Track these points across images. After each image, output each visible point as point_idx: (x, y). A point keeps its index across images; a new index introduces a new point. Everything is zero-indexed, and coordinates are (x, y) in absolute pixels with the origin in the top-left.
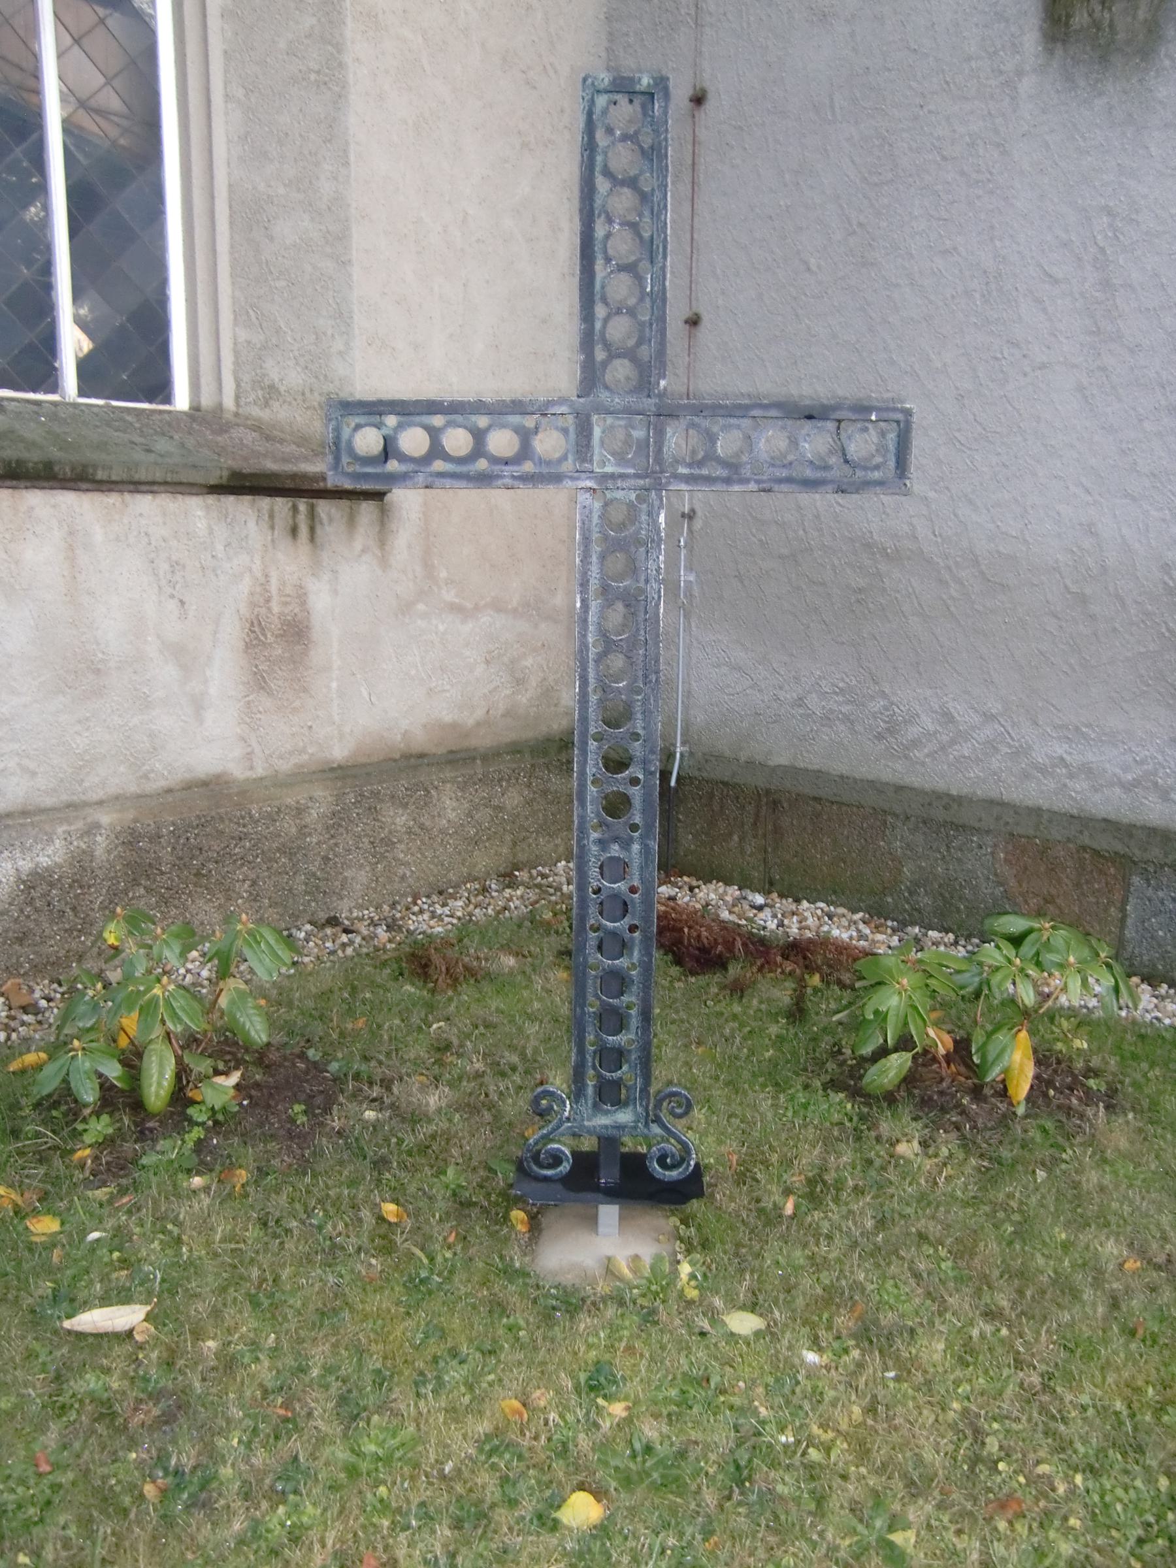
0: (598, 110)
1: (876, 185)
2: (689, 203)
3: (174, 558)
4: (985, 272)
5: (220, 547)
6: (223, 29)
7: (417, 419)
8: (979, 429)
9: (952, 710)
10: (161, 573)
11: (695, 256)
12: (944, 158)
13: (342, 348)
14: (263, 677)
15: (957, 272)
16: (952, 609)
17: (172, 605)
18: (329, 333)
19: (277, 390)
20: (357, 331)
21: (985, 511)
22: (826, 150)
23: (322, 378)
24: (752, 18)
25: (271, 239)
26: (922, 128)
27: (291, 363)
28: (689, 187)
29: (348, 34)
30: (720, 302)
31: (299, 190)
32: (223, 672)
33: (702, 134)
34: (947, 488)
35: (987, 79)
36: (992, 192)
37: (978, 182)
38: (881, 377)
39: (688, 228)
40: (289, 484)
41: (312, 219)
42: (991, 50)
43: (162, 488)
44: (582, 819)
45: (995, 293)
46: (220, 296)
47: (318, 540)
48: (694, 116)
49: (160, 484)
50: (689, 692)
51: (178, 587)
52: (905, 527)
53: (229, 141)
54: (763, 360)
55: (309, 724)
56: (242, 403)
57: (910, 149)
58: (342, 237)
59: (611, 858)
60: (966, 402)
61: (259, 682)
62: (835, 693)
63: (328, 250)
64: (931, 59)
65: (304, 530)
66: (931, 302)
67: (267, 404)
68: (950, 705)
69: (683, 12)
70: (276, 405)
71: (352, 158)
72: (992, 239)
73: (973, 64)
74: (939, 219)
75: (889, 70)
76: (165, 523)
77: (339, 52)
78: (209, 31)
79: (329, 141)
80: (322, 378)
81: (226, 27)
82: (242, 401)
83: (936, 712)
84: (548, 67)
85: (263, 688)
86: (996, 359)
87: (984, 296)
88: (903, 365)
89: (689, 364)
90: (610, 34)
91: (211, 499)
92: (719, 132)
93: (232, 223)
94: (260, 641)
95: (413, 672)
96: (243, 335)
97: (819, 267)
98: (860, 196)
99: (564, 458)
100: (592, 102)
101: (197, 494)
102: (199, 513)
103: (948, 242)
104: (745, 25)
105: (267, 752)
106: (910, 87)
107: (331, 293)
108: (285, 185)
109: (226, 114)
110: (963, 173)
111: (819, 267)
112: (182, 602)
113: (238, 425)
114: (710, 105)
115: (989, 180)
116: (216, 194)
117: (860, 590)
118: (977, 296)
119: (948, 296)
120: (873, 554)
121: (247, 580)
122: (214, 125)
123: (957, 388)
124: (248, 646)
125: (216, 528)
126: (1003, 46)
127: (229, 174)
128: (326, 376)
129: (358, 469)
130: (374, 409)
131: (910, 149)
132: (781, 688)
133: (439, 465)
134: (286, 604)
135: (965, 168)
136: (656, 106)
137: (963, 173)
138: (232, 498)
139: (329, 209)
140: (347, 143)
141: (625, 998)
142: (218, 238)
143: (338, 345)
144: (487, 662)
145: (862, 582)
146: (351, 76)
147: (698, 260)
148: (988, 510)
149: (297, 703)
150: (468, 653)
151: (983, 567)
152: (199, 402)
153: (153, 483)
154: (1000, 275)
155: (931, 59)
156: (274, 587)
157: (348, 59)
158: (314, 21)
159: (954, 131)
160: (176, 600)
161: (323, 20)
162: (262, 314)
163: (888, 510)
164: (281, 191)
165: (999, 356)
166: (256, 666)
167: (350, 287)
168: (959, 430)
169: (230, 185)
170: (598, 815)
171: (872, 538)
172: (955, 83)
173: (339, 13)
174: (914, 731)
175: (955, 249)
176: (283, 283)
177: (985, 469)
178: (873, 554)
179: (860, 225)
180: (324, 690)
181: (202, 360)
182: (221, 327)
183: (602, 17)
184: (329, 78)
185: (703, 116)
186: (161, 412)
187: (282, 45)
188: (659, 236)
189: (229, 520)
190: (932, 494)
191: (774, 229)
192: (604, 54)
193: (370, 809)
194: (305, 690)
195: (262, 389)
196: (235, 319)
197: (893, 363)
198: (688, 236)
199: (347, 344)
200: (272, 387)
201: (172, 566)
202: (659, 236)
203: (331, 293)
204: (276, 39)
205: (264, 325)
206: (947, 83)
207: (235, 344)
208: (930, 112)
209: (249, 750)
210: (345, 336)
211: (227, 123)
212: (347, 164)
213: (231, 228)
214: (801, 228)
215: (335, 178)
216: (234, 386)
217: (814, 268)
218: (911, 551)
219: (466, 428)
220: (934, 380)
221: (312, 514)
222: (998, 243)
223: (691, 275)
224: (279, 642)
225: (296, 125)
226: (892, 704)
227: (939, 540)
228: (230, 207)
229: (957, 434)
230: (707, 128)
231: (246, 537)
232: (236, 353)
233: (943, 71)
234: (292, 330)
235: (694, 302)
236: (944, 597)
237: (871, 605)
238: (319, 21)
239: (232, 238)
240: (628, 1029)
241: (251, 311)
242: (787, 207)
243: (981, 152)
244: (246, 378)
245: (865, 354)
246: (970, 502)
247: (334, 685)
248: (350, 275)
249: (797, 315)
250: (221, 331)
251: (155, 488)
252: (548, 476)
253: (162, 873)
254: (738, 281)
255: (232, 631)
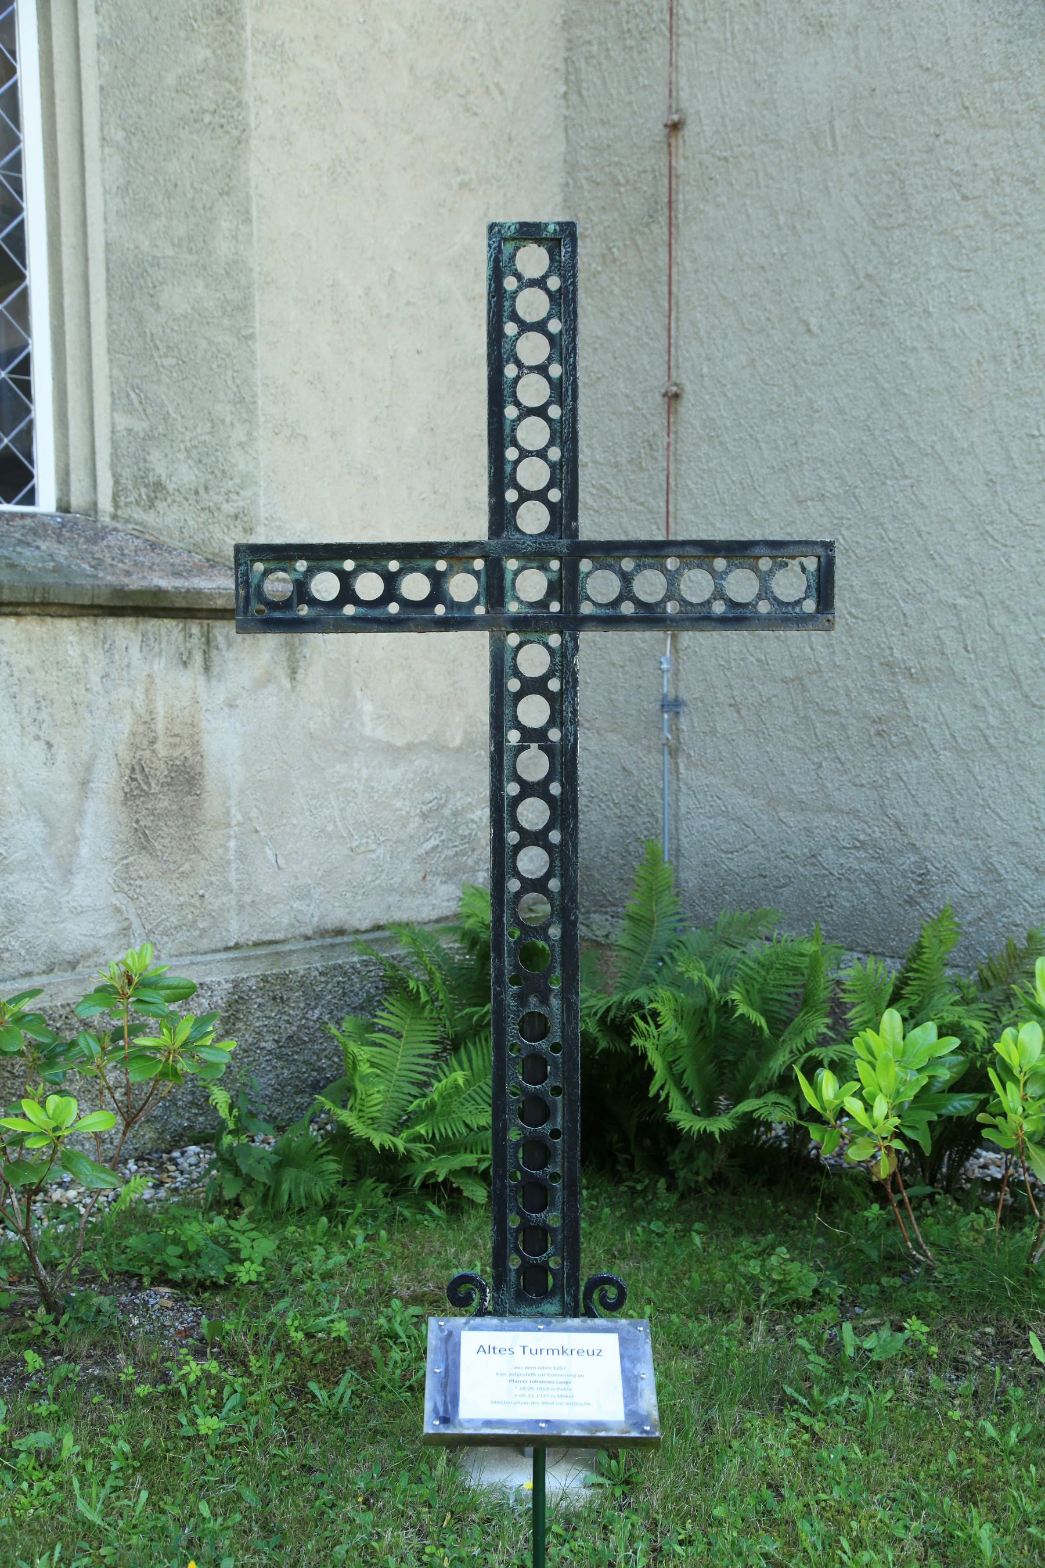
0: (505, 257)
1: (887, 229)
2: (667, 249)
3: (40, 692)
4: (1016, 333)
5: (95, 679)
6: (98, 61)
7: (328, 564)
8: (1015, 521)
9: (998, 866)
10: (25, 712)
11: (674, 313)
12: (965, 198)
13: (244, 439)
14: (145, 836)
15: (983, 333)
16: (992, 741)
17: (37, 749)
18: (228, 419)
19: (165, 488)
20: (262, 419)
21: (1025, 621)
22: (826, 188)
23: (219, 474)
24: (737, 27)
25: (158, 308)
26: (938, 161)
27: (181, 456)
28: (665, 230)
29: (249, 68)
30: (705, 370)
31: (190, 251)
32: (100, 824)
33: (680, 166)
34: (980, 594)
35: (1013, 104)
36: (1021, 237)
37: (1004, 225)
38: (897, 460)
39: (665, 279)
40: (180, 603)
41: (207, 286)
42: (1016, 69)
43: (28, 610)
44: (500, 971)
45: (1028, 359)
46: (95, 377)
47: (216, 670)
48: (669, 145)
49: (25, 604)
50: (678, 850)
51: (44, 726)
52: (931, 641)
53: (106, 192)
54: (757, 441)
55: (201, 892)
56: (122, 504)
57: (926, 187)
58: (244, 307)
59: (531, 1014)
60: (998, 488)
61: (142, 840)
62: (855, 847)
63: (226, 322)
64: (947, 79)
65: (198, 658)
66: (953, 369)
67: (152, 506)
68: (994, 859)
69: (655, 17)
70: (161, 506)
71: (254, 213)
72: (1023, 294)
73: (996, 85)
74: (960, 270)
75: (898, 92)
76: (29, 650)
77: (239, 90)
78: (83, 64)
79: (228, 194)
80: (219, 474)
81: (102, 58)
82: (122, 500)
83: (978, 869)
84: (492, 87)
85: (144, 848)
86: (1033, 436)
87: (1016, 362)
88: (922, 445)
89: (669, 444)
90: (570, 41)
91: (85, 623)
92: (700, 164)
93: (109, 288)
94: (142, 790)
95: (330, 828)
96: (123, 421)
97: (821, 327)
98: (869, 242)
99: (475, 602)
100: (499, 251)
101: (69, 616)
102: (71, 638)
103: (971, 298)
104: (728, 35)
105: (148, 927)
106: (923, 113)
107: (230, 372)
108: (174, 245)
109: (103, 160)
110: (986, 214)
111: (821, 327)
112: (50, 746)
113: (115, 530)
114: (689, 131)
115: (1017, 224)
116: (90, 255)
117: (880, 720)
118: (1008, 361)
119: (974, 361)
120: (894, 674)
121: (128, 717)
122: (87, 175)
123: (988, 473)
124: (128, 797)
125: (91, 656)
126: (1031, 66)
127: (106, 231)
128: (223, 471)
129: (268, 614)
130: (281, 554)
131: (926, 187)
132: (790, 843)
133: (349, 610)
134: (174, 745)
135: (990, 209)
136: (563, 250)
137: (986, 214)
138: (111, 621)
139: (227, 273)
140: (248, 198)
141: (549, 1169)
142: (93, 307)
143: (239, 434)
144: (424, 816)
145: (884, 710)
146: (253, 117)
147: (677, 319)
148: (1029, 619)
149: (187, 867)
150: (399, 804)
151: (1027, 689)
152: (68, 502)
153: (18, 604)
154: (1034, 335)
155: (947, 79)
156: (160, 726)
157: (248, 97)
158: (208, 53)
159: (976, 165)
160: (42, 742)
161: (219, 52)
162: (147, 397)
163: (910, 622)
164: (170, 252)
165: (1036, 433)
166: (137, 821)
167: (254, 367)
168: (992, 523)
169: (107, 244)
170: (516, 966)
171: (892, 655)
172: (975, 109)
173: (238, 44)
174: (953, 892)
175: (979, 305)
176: (172, 361)
177: (1024, 569)
178: (894, 674)
179: (868, 276)
180: (220, 851)
181: (72, 450)
182: (96, 413)
183: (559, 20)
184: (228, 122)
185: (681, 141)
186: (23, 516)
187: (170, 80)
188: (568, 379)
189: (107, 646)
190: (961, 601)
191: (768, 282)
192: (561, 66)
193: (274, 999)
194: (197, 850)
195: (146, 486)
196: (113, 403)
197: (909, 442)
198: (665, 289)
199: (249, 434)
200: (159, 486)
201: (38, 702)
202: (568, 379)
203: (230, 372)
204: (164, 73)
205: (149, 411)
206: (966, 108)
207: (113, 432)
208: (947, 142)
209: (126, 924)
210: (247, 425)
211: (103, 170)
212: (248, 221)
213: (108, 294)
214: (799, 281)
215: (235, 237)
216: (111, 483)
217: (815, 329)
218: (939, 670)
219: (376, 572)
220: (960, 463)
221: (208, 640)
222: (1030, 299)
223: (669, 337)
224: (163, 791)
225: (187, 174)
226: (925, 859)
227: (972, 656)
228: (108, 270)
229: (989, 528)
230: (686, 158)
231: (128, 666)
232: (115, 445)
233: (961, 94)
234: (183, 417)
235: (673, 371)
236: (982, 725)
237: (894, 738)
238: (214, 52)
239: (109, 307)
240: (553, 1205)
241: (133, 395)
242: (782, 255)
243: (1008, 190)
244: (126, 473)
245: (877, 432)
246: (1008, 610)
247: (232, 844)
248: (253, 352)
249: (796, 386)
250: (96, 419)
251: (20, 610)
252: (459, 620)
253: (15, 1077)
254: (726, 345)
255: (108, 780)
